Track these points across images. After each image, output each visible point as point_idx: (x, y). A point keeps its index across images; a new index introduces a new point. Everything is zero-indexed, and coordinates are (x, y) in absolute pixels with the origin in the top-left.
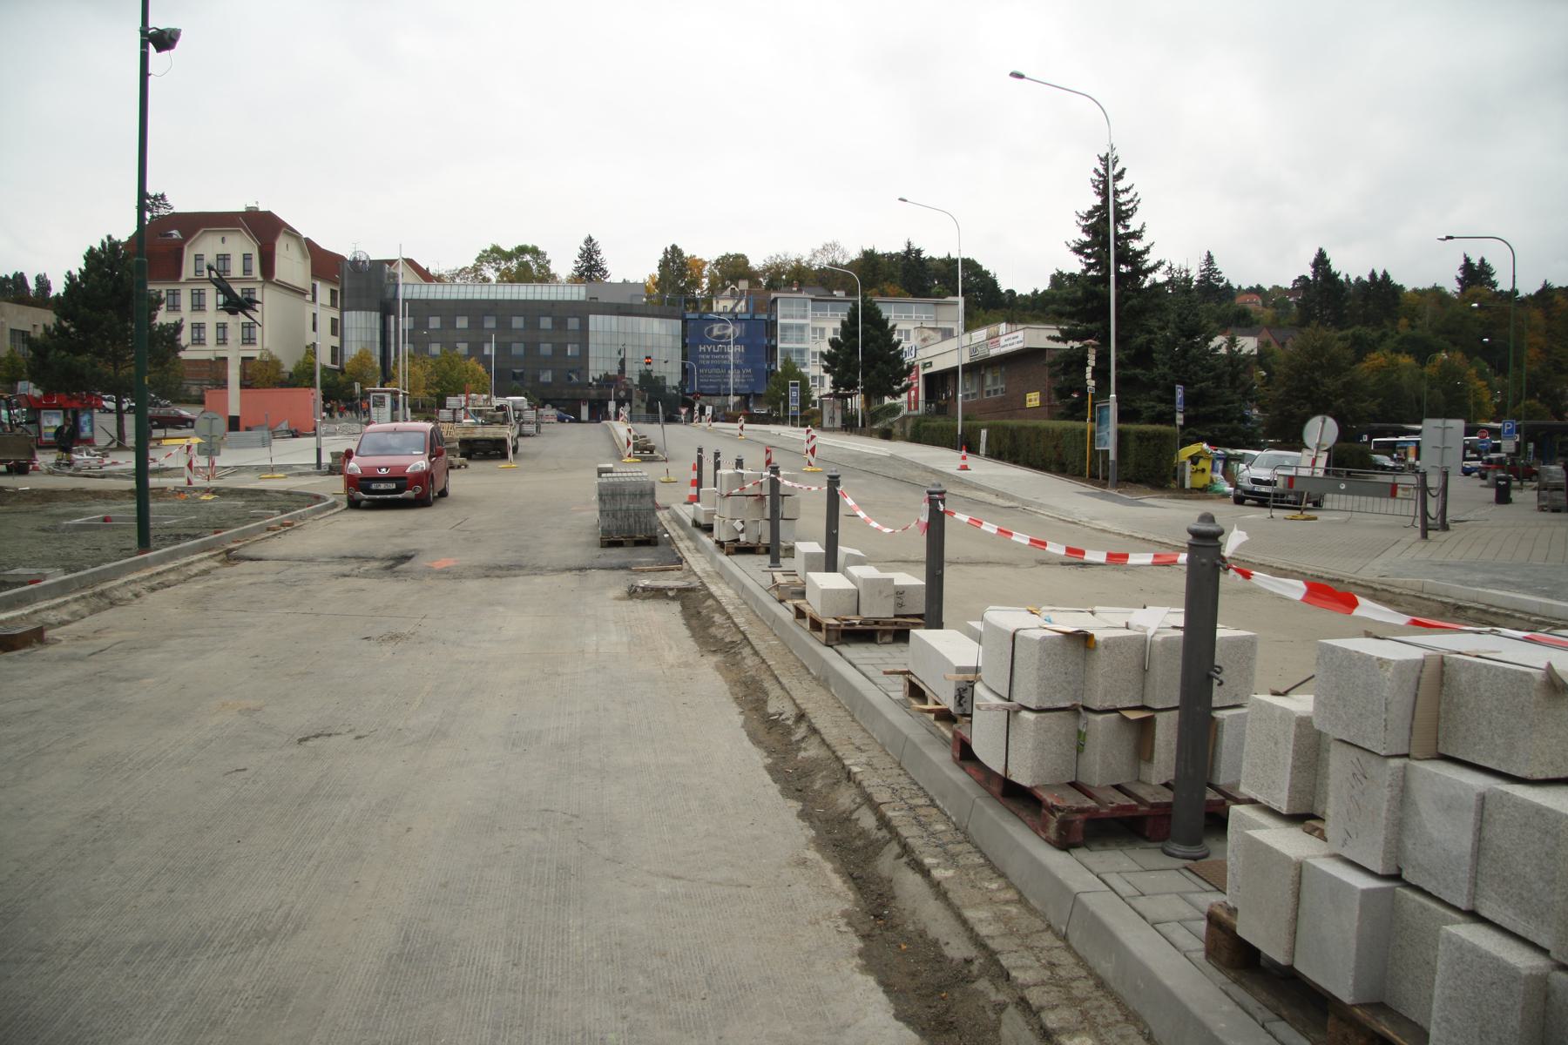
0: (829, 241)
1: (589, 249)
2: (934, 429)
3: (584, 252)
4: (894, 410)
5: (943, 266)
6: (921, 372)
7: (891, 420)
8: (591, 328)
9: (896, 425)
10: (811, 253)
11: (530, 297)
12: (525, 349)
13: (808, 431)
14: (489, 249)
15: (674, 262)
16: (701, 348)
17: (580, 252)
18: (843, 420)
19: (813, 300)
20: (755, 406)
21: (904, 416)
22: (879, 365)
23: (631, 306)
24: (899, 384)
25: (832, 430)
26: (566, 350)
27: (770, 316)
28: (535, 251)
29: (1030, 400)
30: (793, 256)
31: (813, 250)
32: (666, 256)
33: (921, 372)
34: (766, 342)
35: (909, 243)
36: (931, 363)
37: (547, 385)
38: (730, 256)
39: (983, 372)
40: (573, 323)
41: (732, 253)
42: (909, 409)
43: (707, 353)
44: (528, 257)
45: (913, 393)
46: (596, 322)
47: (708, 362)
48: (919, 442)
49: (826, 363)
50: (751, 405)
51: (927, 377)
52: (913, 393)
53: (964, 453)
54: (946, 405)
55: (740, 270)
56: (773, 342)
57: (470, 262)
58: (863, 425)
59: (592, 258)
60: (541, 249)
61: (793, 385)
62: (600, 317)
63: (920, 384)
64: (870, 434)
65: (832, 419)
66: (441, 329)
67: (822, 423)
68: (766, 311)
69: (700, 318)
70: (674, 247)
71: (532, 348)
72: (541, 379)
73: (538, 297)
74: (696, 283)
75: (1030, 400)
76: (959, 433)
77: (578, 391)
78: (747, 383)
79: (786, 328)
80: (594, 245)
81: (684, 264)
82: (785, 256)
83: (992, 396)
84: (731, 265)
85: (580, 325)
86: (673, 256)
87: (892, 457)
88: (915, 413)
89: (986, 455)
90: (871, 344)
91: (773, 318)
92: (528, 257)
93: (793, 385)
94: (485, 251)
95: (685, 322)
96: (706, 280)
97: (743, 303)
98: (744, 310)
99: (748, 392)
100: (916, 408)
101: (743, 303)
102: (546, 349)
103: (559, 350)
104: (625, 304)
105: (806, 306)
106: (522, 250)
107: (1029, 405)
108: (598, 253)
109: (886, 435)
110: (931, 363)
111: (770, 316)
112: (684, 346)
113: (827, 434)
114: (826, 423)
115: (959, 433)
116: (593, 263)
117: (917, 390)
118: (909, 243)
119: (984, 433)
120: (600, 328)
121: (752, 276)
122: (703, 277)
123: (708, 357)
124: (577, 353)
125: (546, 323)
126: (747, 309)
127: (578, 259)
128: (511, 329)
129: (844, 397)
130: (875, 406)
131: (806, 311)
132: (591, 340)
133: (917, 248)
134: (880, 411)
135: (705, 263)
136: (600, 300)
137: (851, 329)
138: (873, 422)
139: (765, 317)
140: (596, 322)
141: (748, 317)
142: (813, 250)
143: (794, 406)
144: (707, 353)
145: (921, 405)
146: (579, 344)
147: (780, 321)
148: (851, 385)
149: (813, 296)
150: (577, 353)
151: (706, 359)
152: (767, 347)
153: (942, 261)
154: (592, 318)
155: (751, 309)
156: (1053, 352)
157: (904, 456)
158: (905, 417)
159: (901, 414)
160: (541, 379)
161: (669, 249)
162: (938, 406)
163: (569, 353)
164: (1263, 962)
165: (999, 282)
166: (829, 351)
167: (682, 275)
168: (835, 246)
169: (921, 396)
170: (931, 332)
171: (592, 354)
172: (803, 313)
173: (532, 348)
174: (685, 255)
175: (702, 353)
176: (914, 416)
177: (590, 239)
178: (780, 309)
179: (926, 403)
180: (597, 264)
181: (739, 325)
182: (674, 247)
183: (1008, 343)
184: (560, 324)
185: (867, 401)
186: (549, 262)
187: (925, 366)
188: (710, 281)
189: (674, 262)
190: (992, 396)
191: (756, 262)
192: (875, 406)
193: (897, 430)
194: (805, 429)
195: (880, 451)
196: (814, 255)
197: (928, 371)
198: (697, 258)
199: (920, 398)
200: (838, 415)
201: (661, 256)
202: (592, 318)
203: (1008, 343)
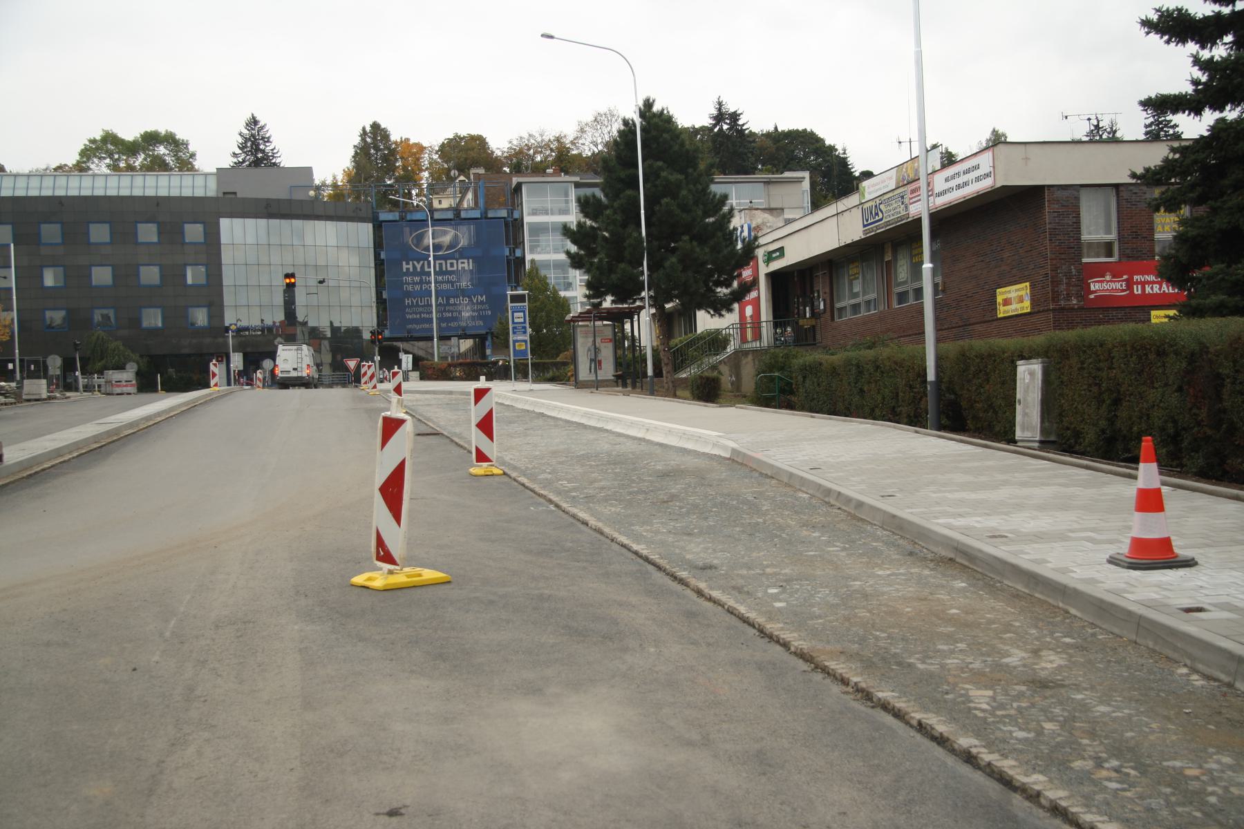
0: (603, 110)
1: (253, 136)
2: (834, 371)
3: (246, 140)
4: (716, 341)
5: (769, 143)
6: (764, 270)
7: (714, 360)
8: (224, 239)
9: (725, 369)
10: (578, 128)
11: (125, 192)
12: (115, 276)
13: (480, 394)
14: (98, 138)
15: (377, 149)
16: (405, 266)
17: (240, 140)
18: (618, 363)
19: (578, 185)
20: (493, 354)
21: (736, 353)
22: (685, 243)
23: (290, 202)
24: (728, 285)
25: (596, 385)
26: (185, 276)
27: (511, 213)
28: (170, 140)
29: (1007, 302)
30: (550, 135)
31: (580, 123)
32: (363, 140)
33: (764, 270)
34: (507, 253)
35: (720, 104)
36: (781, 250)
37: (153, 332)
38: (462, 139)
39: (888, 257)
40: (194, 232)
41: (463, 133)
42: (744, 340)
43: (415, 273)
44: (162, 150)
45: (749, 310)
46: (233, 230)
47: (417, 288)
48: (790, 406)
49: (573, 249)
50: (488, 352)
51: (774, 277)
52: (749, 310)
53: (1148, 474)
54: (814, 327)
55: (472, 154)
56: (518, 253)
57: (72, 159)
58: (658, 372)
59: (258, 150)
60: (180, 136)
61: (515, 299)
62: (237, 222)
63: (763, 292)
64: (672, 392)
65: (596, 363)
66: (42, 267)
67: (575, 374)
68: (502, 205)
69: (402, 218)
70: (375, 126)
71: (125, 274)
72: (145, 324)
73: (137, 192)
74: (410, 178)
75: (1007, 302)
76: (931, 376)
77: (208, 340)
78: (481, 317)
79: (538, 229)
80: (262, 128)
81: (393, 152)
82: (542, 135)
83: (863, 313)
84: (467, 149)
85: (206, 234)
86: (374, 138)
87: (738, 462)
88: (756, 345)
89: (1045, 444)
90: (665, 200)
91: (516, 215)
92: (162, 150)
93: (515, 299)
94: (93, 141)
95: (378, 226)
96: (426, 174)
97: (470, 196)
98: (472, 204)
99: (483, 332)
100: (758, 336)
101: (470, 196)
102: (150, 275)
103: (172, 275)
104: (278, 201)
105: (566, 195)
106: (151, 139)
107: (1002, 312)
108: (267, 140)
109: (707, 391)
110: (781, 250)
111: (511, 213)
112: (379, 264)
113: (584, 395)
114: (584, 373)
115: (931, 376)
116: (260, 155)
117: (756, 303)
118: (720, 104)
119: (1029, 375)
120: (238, 239)
121: (491, 163)
122: (421, 170)
123: (417, 279)
124: (203, 281)
125: (148, 233)
126: (476, 203)
127: (238, 151)
128: (89, 244)
129: (617, 317)
130: (679, 340)
131: (567, 202)
132: (226, 258)
133: (732, 110)
134: (690, 344)
135: (421, 149)
136: (239, 195)
137: (623, 174)
138: (677, 368)
139: (503, 213)
140: (233, 230)
141: (477, 214)
142: (580, 123)
143: (520, 340)
144: (415, 273)
145: (766, 330)
146: (206, 265)
147: (527, 219)
148: (626, 291)
149: (577, 179)
150: (203, 281)
151: (414, 283)
152: (509, 262)
153: (768, 135)
154: (225, 223)
155: (481, 202)
156: (1059, 194)
157: (780, 458)
158: (739, 354)
159: (730, 349)
160: (145, 324)
161: (368, 129)
162: (798, 329)
163: (189, 281)
164: (687, 393)
165: (851, 161)
166: (580, 225)
167: (390, 169)
168: (613, 116)
169: (766, 313)
170: (767, 216)
171: (227, 280)
172: (563, 205)
173: (125, 274)
174: (393, 138)
175: (408, 273)
176: (754, 351)
177: (253, 122)
178: (528, 201)
179: (776, 325)
180: (266, 157)
181: (464, 229)
182: (375, 126)
183: (953, 183)
184: (171, 231)
185: (665, 322)
186: (193, 155)
187: (769, 258)
188: (431, 175)
189: (377, 149)
190: (863, 313)
191: (499, 144)
192: (679, 340)
193: (726, 379)
194: (471, 386)
195: (699, 439)
196: (582, 131)
197: (776, 265)
198: (411, 142)
199: (763, 318)
200: (607, 353)
201: (357, 140)
202: (225, 223)
203: (953, 183)
